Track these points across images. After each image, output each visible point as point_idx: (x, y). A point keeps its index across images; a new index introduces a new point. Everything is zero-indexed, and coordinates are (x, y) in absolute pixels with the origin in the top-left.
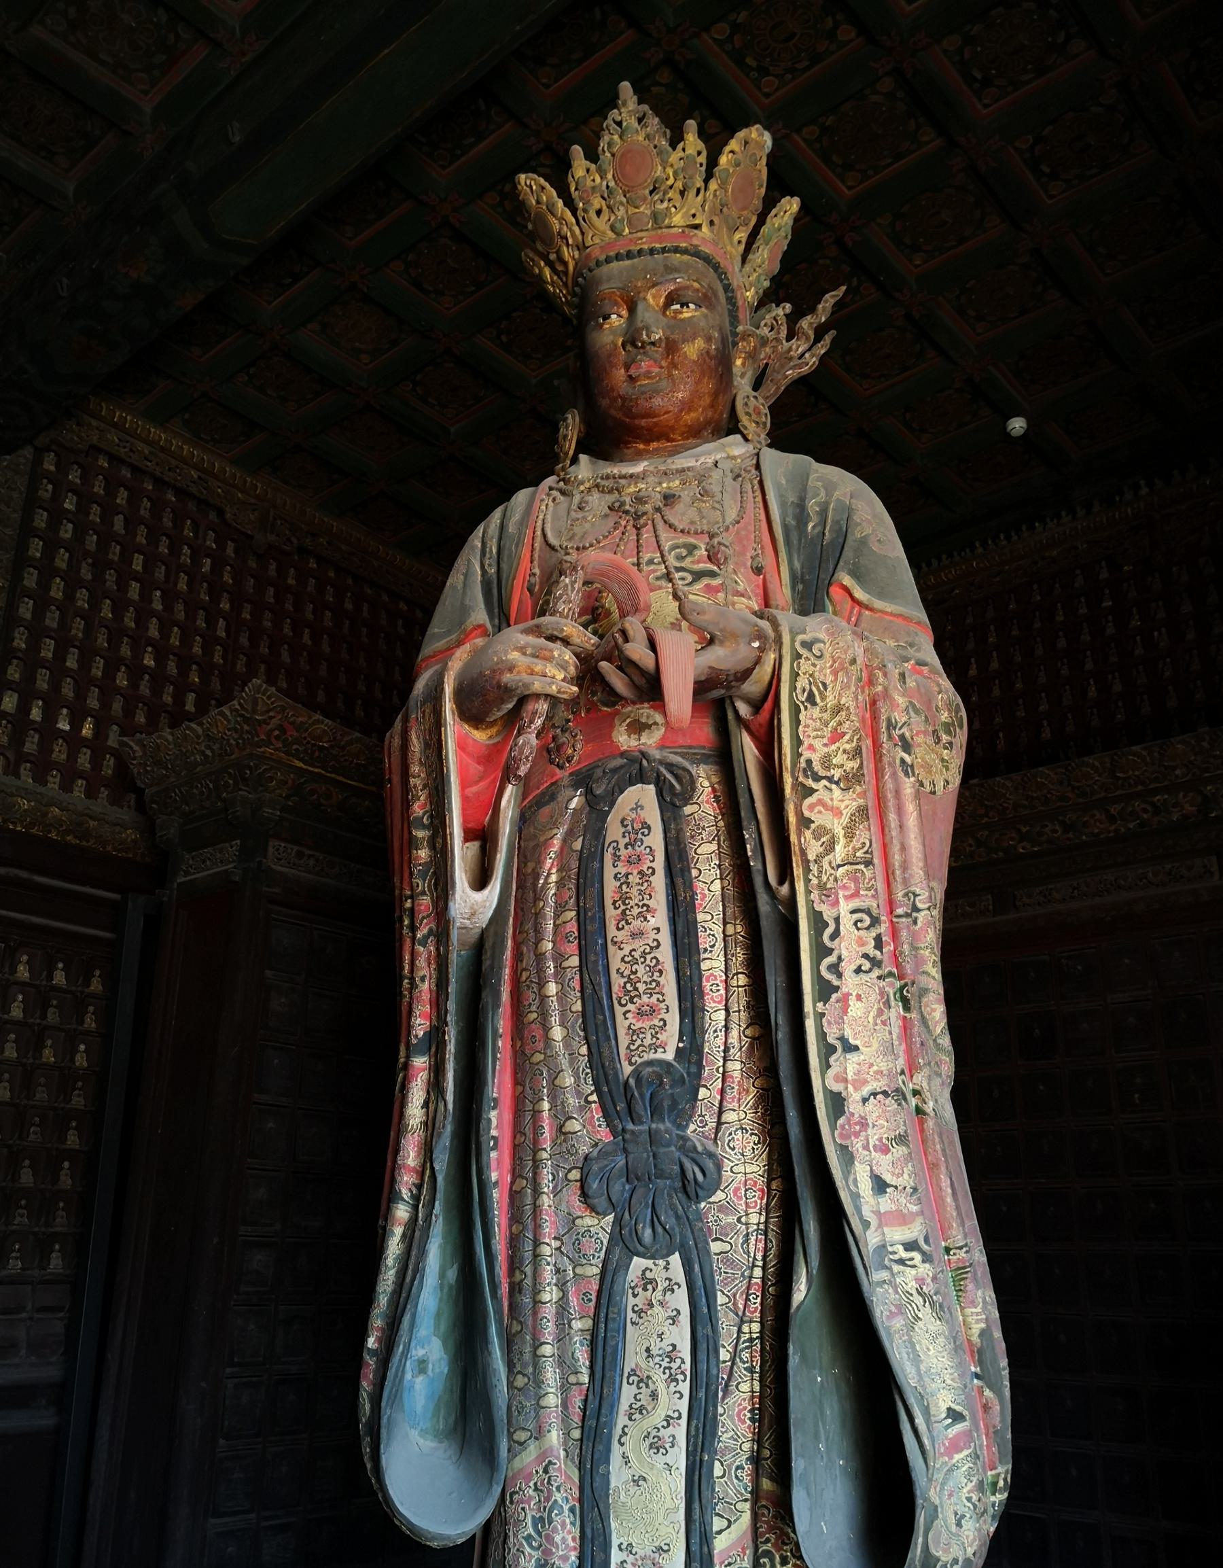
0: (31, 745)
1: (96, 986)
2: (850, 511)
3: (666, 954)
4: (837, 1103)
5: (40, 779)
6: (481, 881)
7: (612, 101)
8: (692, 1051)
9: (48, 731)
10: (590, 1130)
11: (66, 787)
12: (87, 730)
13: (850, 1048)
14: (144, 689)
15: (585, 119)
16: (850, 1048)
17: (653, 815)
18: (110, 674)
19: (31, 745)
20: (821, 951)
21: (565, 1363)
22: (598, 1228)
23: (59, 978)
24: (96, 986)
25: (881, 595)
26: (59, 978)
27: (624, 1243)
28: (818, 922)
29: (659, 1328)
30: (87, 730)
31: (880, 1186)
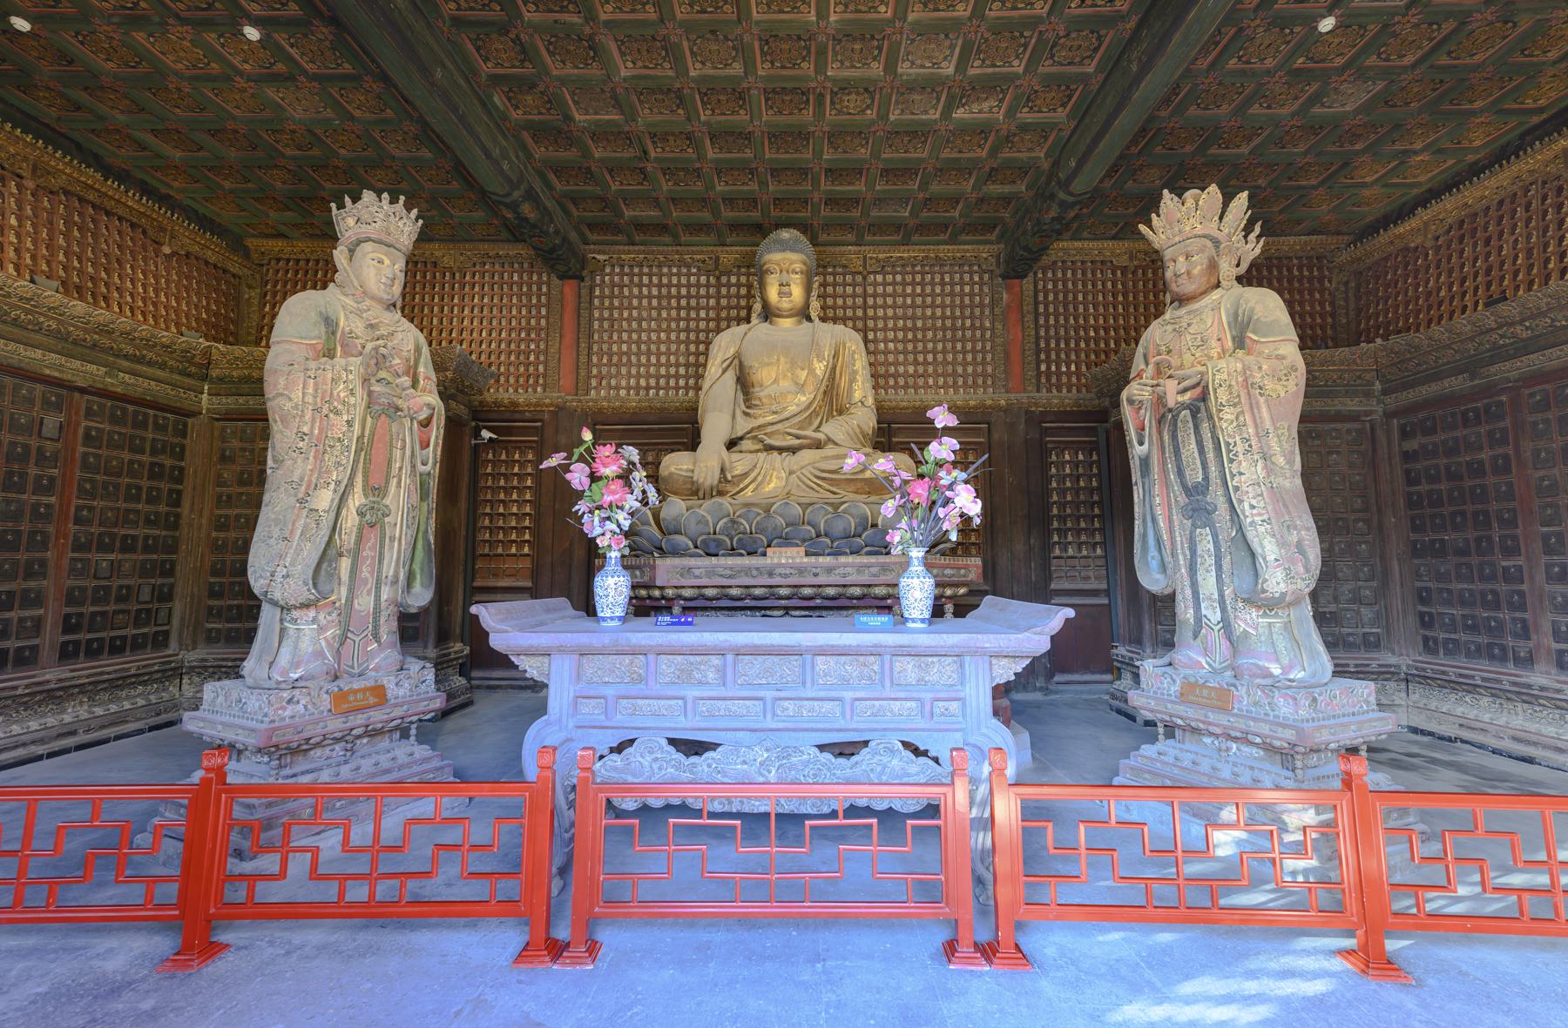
0: (1054, 380)
1: (1095, 457)
2: (1252, 310)
3: (1196, 454)
4: (1237, 489)
5: (1059, 390)
6: (1141, 443)
7: (1160, 197)
8: (1206, 478)
9: (1059, 373)
10: (1183, 499)
11: (1069, 391)
12: (1073, 368)
13: (1241, 474)
14: (1092, 345)
15: (1153, 204)
16: (1241, 474)
17: (1189, 418)
18: (1077, 344)
19: (1054, 380)
20: (1229, 451)
21: (1184, 554)
22: (1188, 523)
23: (1081, 457)
24: (1095, 457)
25: (1264, 336)
26: (1081, 457)
27: (1194, 526)
28: (1228, 444)
29: (1206, 544)
30: (1073, 368)
31: (1253, 507)
